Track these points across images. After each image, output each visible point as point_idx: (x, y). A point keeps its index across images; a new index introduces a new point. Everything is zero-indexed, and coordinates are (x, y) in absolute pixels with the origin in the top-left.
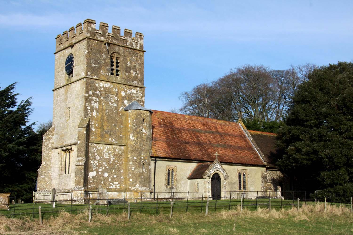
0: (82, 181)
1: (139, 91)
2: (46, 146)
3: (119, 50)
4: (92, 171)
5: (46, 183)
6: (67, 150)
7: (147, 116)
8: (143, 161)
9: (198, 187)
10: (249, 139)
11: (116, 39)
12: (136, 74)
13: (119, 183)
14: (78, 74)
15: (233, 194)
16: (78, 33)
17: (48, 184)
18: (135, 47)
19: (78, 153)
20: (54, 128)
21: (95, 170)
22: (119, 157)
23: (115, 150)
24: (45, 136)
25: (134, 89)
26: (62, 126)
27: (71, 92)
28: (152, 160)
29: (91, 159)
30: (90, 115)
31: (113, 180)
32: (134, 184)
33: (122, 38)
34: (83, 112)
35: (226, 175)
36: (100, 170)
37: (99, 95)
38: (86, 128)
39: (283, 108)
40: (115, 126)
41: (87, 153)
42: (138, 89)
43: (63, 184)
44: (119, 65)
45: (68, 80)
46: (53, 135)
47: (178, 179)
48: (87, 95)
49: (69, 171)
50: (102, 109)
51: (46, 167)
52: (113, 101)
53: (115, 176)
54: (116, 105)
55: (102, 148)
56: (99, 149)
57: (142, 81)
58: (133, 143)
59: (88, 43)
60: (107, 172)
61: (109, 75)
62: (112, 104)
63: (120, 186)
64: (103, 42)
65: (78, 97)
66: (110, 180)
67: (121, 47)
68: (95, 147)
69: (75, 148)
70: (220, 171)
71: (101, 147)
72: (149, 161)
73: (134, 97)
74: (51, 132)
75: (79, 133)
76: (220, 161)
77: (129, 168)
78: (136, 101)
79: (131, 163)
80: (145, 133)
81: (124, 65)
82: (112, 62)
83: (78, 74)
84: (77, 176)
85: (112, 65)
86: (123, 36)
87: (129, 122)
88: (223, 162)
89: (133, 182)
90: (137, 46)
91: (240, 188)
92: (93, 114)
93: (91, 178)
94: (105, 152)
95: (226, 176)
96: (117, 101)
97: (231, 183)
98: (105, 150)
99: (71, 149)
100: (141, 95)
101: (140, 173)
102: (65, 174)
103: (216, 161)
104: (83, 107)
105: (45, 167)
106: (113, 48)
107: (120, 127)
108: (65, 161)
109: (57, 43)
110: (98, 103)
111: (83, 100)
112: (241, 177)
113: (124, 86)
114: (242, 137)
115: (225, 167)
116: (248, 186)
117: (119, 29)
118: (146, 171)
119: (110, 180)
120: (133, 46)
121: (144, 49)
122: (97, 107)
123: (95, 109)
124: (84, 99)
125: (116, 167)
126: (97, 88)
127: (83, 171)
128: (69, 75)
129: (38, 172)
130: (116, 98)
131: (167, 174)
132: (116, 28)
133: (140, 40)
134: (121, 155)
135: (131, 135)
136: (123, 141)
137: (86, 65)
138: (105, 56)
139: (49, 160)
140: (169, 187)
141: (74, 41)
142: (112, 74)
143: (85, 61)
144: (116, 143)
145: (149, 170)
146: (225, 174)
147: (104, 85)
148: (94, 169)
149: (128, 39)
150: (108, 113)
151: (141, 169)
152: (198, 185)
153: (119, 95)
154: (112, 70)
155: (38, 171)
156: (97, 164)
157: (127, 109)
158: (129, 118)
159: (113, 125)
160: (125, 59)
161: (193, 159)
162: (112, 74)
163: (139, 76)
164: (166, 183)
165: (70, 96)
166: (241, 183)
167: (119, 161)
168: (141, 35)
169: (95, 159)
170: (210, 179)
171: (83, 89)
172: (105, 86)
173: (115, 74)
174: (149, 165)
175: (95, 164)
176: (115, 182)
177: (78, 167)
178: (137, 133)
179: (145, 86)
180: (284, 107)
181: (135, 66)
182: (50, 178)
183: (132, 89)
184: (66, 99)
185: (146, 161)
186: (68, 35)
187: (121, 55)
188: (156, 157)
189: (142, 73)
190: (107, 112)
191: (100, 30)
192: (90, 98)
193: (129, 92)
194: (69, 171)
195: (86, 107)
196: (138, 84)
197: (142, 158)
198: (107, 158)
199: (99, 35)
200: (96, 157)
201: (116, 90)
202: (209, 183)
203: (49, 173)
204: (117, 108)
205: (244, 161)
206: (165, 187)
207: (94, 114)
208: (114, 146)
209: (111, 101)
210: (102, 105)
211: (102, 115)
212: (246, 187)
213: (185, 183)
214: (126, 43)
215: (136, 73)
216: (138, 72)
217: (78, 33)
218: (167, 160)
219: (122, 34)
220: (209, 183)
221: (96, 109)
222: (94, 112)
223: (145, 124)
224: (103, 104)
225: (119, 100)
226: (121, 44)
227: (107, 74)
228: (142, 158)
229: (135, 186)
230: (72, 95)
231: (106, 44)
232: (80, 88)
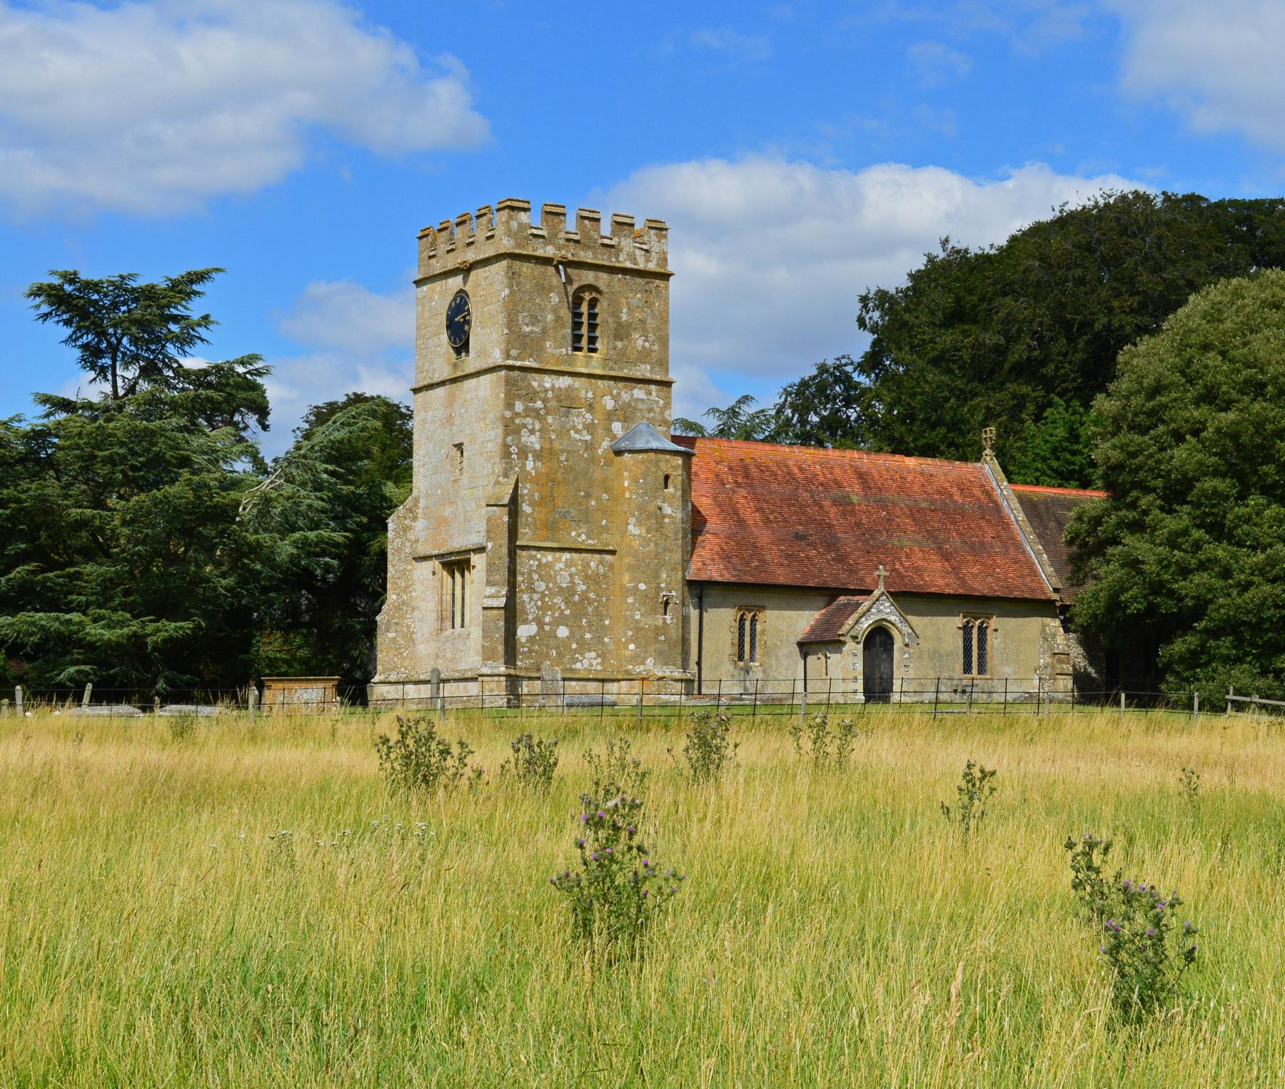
0: (501, 648)
2: (398, 550)
4: (526, 622)
5: (401, 654)
6: (456, 564)
8: (664, 593)
10: (1015, 513)
12: (647, 344)
13: (599, 656)
14: (483, 353)
15: (493, 685)
16: (481, 235)
18: (641, 266)
19: (488, 576)
20: (417, 500)
21: (533, 620)
22: (597, 583)
23: (586, 565)
24: (393, 521)
25: (640, 389)
26: (442, 493)
29: (522, 591)
30: (517, 469)
31: (583, 647)
32: (638, 659)
33: (606, 241)
34: (497, 460)
35: (910, 631)
36: (547, 619)
37: (542, 412)
38: (507, 508)
41: (512, 572)
42: (653, 387)
45: (455, 366)
47: (768, 642)
48: (508, 414)
49: (463, 621)
50: (551, 451)
51: (398, 608)
52: (580, 427)
53: (588, 636)
54: (588, 437)
56: (544, 561)
57: (663, 363)
59: (509, 267)
60: (567, 626)
61: (567, 354)
62: (577, 436)
63: (602, 664)
65: (484, 419)
69: (476, 559)
73: (641, 410)
74: (410, 510)
75: (489, 520)
78: (645, 421)
79: (630, 600)
80: (670, 516)
81: (610, 320)
82: (577, 315)
84: (486, 634)
86: (609, 235)
87: (626, 484)
91: (967, 669)
93: (523, 640)
94: (561, 570)
99: (468, 561)
102: (453, 627)
104: (499, 445)
105: (395, 607)
107: (599, 500)
108: (450, 592)
109: (421, 252)
110: (538, 433)
113: (612, 383)
114: (993, 511)
116: (994, 658)
117: (595, 216)
118: (675, 620)
119: (574, 646)
121: (670, 269)
125: (590, 609)
126: (536, 392)
127: (502, 623)
128: (458, 351)
130: (588, 416)
135: (632, 520)
136: (611, 542)
137: (506, 331)
138: (557, 300)
139: (405, 590)
141: (471, 256)
143: (502, 319)
148: (530, 617)
149: (623, 244)
153: (597, 407)
155: (378, 618)
156: (539, 603)
158: (626, 474)
167: (598, 595)
168: (659, 225)
169: (534, 591)
170: (861, 646)
171: (497, 396)
172: (557, 386)
173: (586, 349)
175: (532, 603)
176: (589, 651)
177: (489, 613)
179: (671, 376)
182: (410, 639)
183: (634, 388)
185: (674, 593)
186: (452, 233)
189: (664, 342)
190: (563, 458)
192: (517, 421)
193: (625, 396)
194: (463, 621)
195: (506, 446)
198: (564, 585)
200: (536, 583)
201: (590, 395)
203: (408, 626)
204: (590, 446)
207: (530, 465)
209: (574, 428)
210: (551, 441)
212: (989, 666)
216: (652, 337)
217: (481, 235)
219: (606, 228)
222: (527, 459)
224: (553, 437)
225: (596, 421)
227: (564, 351)
229: (643, 663)
231: (560, 267)
232: (489, 393)
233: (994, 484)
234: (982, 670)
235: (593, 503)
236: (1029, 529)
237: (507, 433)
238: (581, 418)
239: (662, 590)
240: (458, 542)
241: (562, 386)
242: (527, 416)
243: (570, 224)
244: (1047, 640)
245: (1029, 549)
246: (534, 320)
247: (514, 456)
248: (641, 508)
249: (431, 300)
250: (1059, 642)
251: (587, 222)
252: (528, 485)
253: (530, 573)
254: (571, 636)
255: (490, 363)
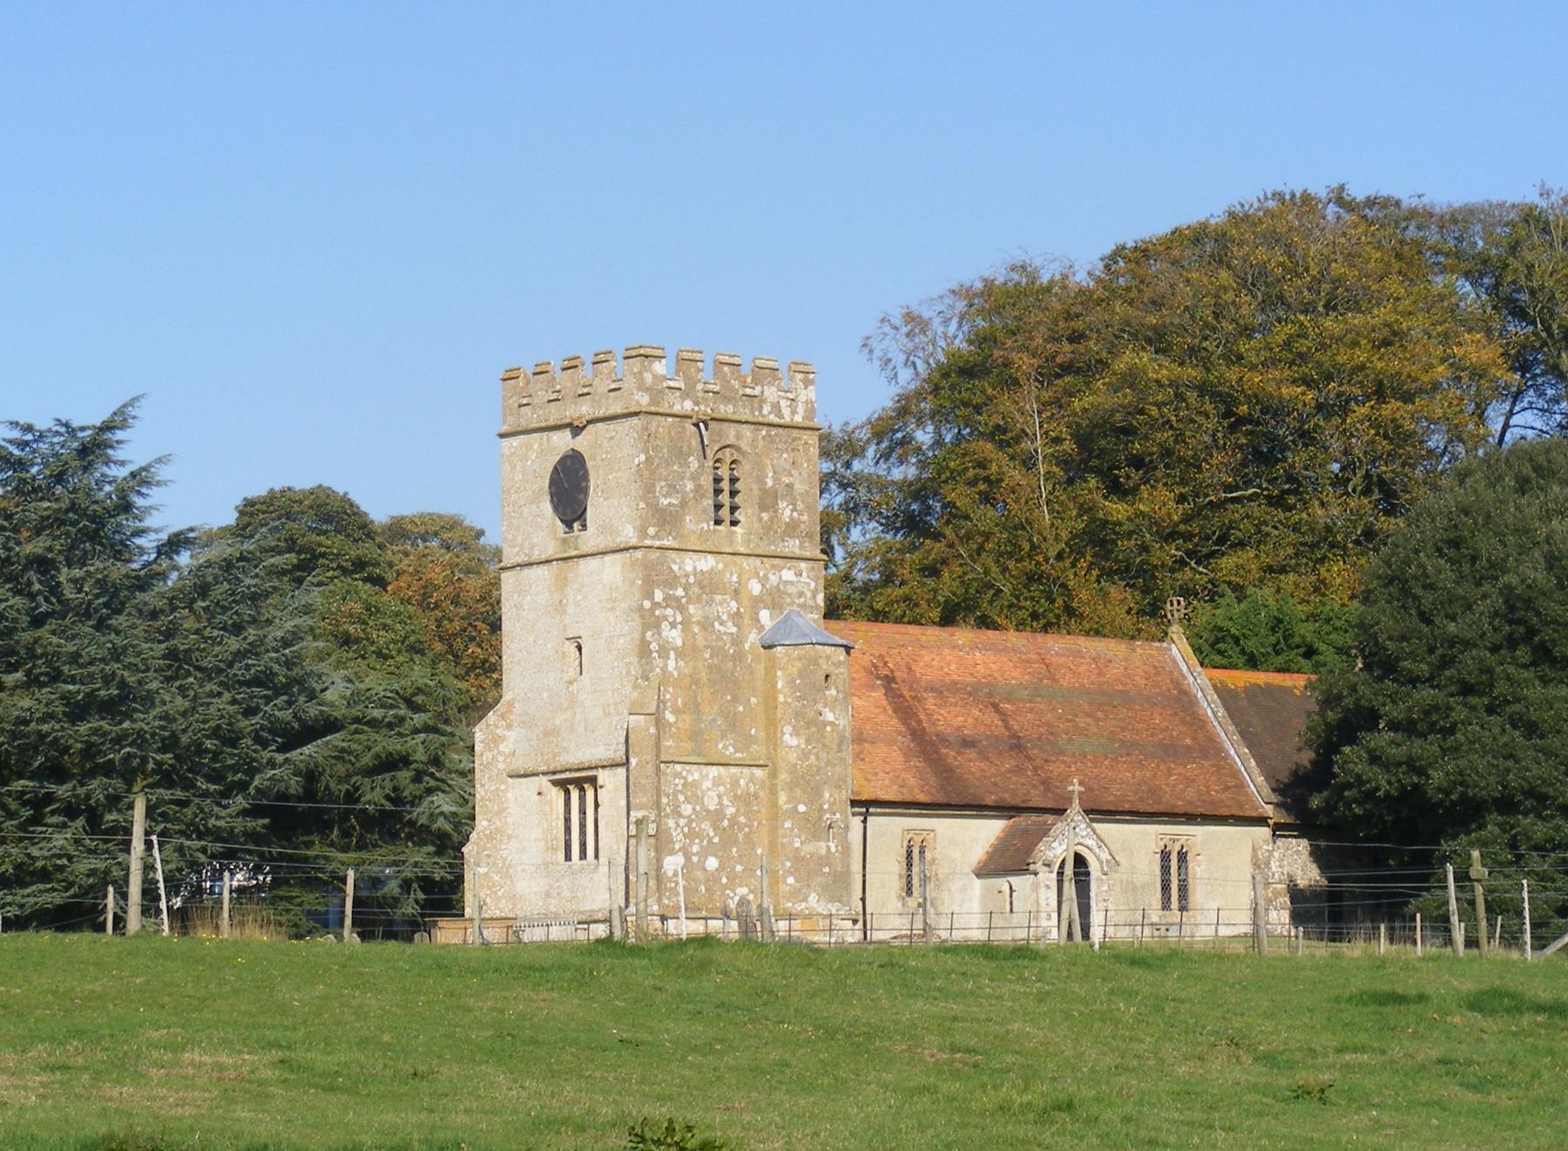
1: (804, 574)
3: (738, 437)
4: (672, 852)
5: (496, 893)
7: (838, 664)
9: (1011, 903)
10: (1210, 707)
11: (727, 399)
12: (795, 514)
14: (605, 529)
17: (500, 893)
18: (787, 420)
20: (511, 704)
21: (680, 850)
23: (735, 783)
27: (582, 586)
28: (854, 814)
32: (799, 894)
35: (1109, 857)
36: (695, 849)
39: (1506, 427)
40: (735, 699)
42: (803, 565)
43: (566, 894)
44: (738, 486)
45: (564, 541)
46: (509, 727)
48: (647, 604)
49: (597, 849)
51: (490, 837)
52: (725, 617)
53: (739, 868)
54: (734, 630)
55: (696, 776)
56: (690, 779)
58: (793, 757)
60: (716, 856)
62: (722, 629)
64: (691, 417)
66: (724, 880)
67: (745, 426)
68: (678, 775)
70: (1087, 847)
71: (694, 774)
72: (847, 817)
73: (790, 595)
74: (503, 717)
76: (1090, 806)
77: (785, 840)
78: (795, 608)
79: (788, 825)
80: (832, 723)
83: (605, 529)
85: (718, 492)
87: (780, 685)
88: (1098, 812)
89: (798, 885)
90: (794, 412)
91: (1166, 906)
92: (666, 665)
95: (1108, 861)
96: (738, 613)
97: (1131, 888)
98: (707, 784)
100: (813, 584)
101: (820, 857)
103: (1075, 811)
104: (638, 642)
105: (487, 837)
106: (720, 434)
109: (505, 398)
110: (680, 626)
111: (633, 620)
112: (1173, 867)
113: (758, 561)
114: (1184, 702)
115: (1106, 829)
116: (1198, 895)
117: (736, 361)
119: (724, 880)
120: (781, 417)
122: (679, 643)
123: (673, 649)
124: (638, 621)
125: (741, 836)
128: (568, 524)
129: (466, 856)
130: (734, 604)
131: (904, 859)
132: (726, 359)
133: (806, 388)
134: (756, 796)
135: (788, 729)
140: (912, 903)
141: (585, 409)
142: (718, 522)
144: (740, 759)
145: (846, 848)
146: (1105, 856)
147: (697, 564)
148: (677, 846)
149: (766, 393)
150: (711, 657)
151: (823, 844)
152: (1011, 896)
154: (718, 507)
156: (686, 830)
157: (769, 642)
158: (779, 673)
159: (729, 697)
160: (759, 466)
161: (991, 803)
162: (718, 522)
163: (805, 518)
164: (902, 889)
165: (579, 598)
166: (849, 855)
167: (749, 819)
169: (680, 815)
171: (632, 583)
174: (847, 828)
175: (679, 830)
178: (808, 725)
180: (1514, 420)
181: (790, 486)
184: (560, 608)
185: (838, 815)
187: (744, 454)
188: (867, 804)
190: (707, 656)
191: (677, 373)
192: (657, 613)
193: (773, 579)
194: (597, 849)
196: (801, 546)
197: (826, 806)
198: (712, 808)
199: (678, 393)
201: (735, 578)
202: (1048, 887)
203: (504, 860)
204: (737, 641)
205: (1180, 805)
206: (900, 904)
207: (671, 664)
208: (733, 770)
211: (694, 668)
213: (964, 889)
214: (761, 408)
215: (792, 511)
216: (800, 506)
218: (887, 810)
220: (1048, 887)
221: (675, 649)
223: (833, 692)
225: (742, 610)
226: (745, 414)
228: (826, 806)
229: (805, 900)
230: (585, 597)
231: (701, 425)
233: (1185, 669)
234: (1183, 909)
235: (741, 708)
236: (1232, 728)
237: (646, 627)
238: (725, 606)
239: (826, 811)
240: (577, 754)
241: (705, 569)
242: (668, 606)
243: (707, 373)
244: (1259, 867)
245: (1232, 752)
246: (672, 489)
247: (655, 655)
248: (799, 714)
249: (525, 458)
250: (1274, 869)
251: (726, 369)
252: (671, 689)
253: (676, 793)
254: (721, 868)
255: (620, 541)
